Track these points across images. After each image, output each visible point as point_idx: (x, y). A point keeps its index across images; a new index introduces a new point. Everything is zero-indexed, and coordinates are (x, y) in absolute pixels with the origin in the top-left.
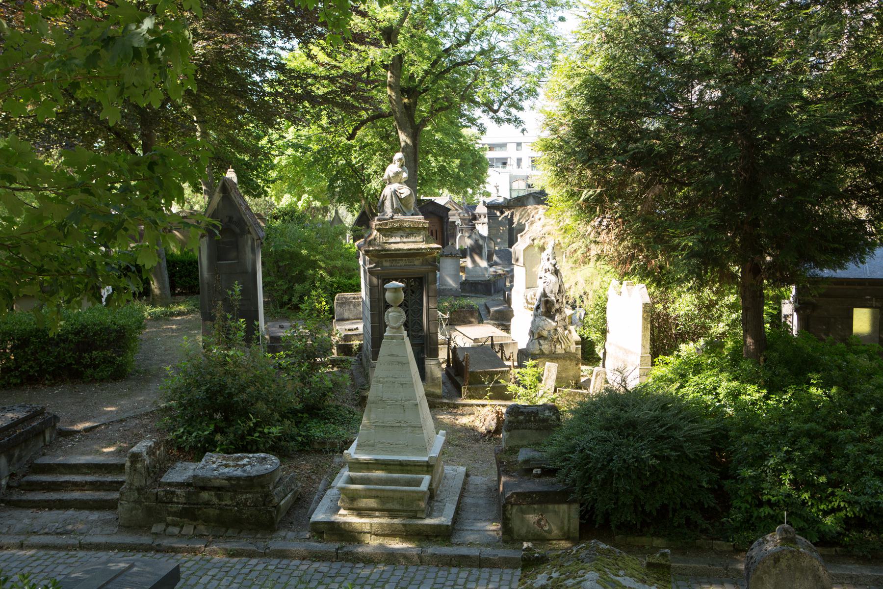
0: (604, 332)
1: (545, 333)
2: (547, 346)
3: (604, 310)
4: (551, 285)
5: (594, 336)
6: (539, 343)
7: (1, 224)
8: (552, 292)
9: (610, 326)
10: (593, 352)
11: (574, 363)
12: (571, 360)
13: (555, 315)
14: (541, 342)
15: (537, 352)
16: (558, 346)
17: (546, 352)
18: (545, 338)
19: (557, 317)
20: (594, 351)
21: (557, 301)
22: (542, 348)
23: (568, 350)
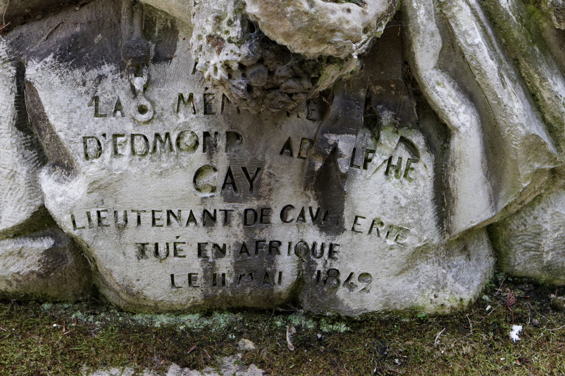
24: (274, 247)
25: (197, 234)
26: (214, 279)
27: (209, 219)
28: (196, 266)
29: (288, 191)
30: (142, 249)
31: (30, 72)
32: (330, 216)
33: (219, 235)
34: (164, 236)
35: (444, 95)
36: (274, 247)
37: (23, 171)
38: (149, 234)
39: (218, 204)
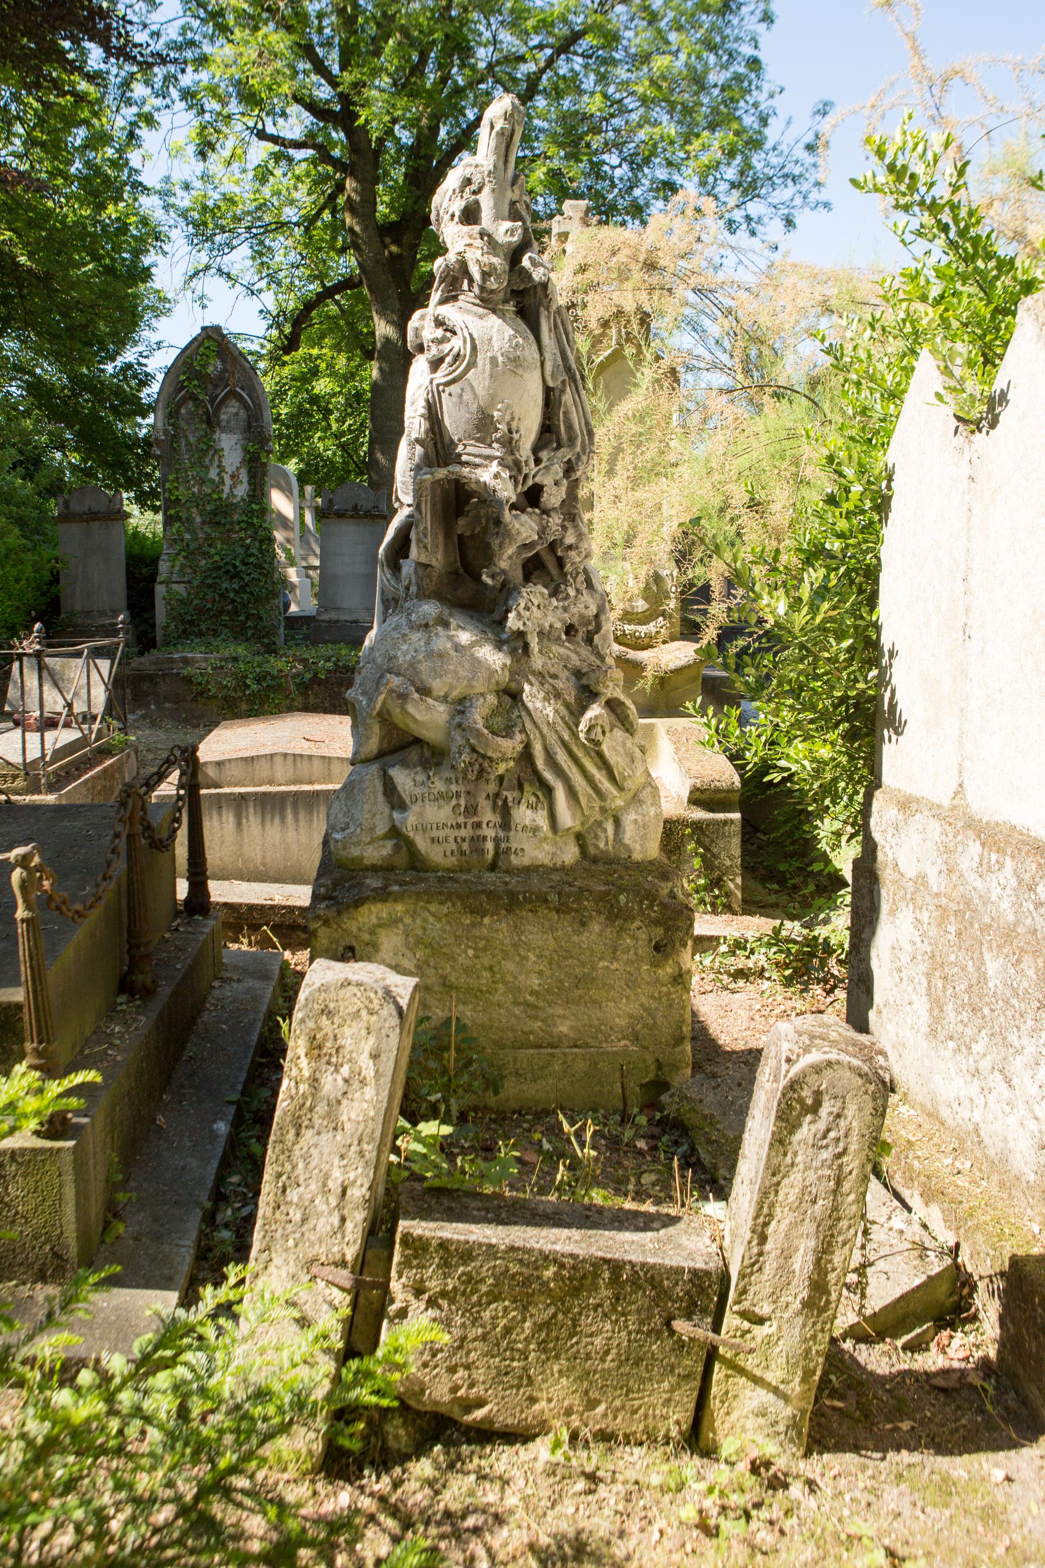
0: (867, 722)
1: (429, 718)
2: (440, 814)
3: (864, 582)
4: (479, 378)
5: (807, 756)
6: (390, 789)
7: (8, 498)
8: (483, 426)
9: (908, 686)
10: (805, 848)
11: (639, 936)
12: (616, 915)
13: (506, 591)
14: (402, 778)
15: (375, 853)
16: (525, 815)
17: (437, 855)
18: (430, 756)
19: (532, 610)
20: (809, 844)
21: (532, 497)
22: (409, 821)
23: (604, 841)
24: (485, 838)
25: (452, 833)
26: (462, 853)
27: (459, 826)
28: (454, 847)
29: (488, 815)
30: (433, 840)
31: (242, 490)
32: (506, 824)
33: (463, 833)
34: (441, 834)
35: (548, 776)
36: (485, 838)
37: (387, 811)
38: (435, 833)
39: (461, 820)
